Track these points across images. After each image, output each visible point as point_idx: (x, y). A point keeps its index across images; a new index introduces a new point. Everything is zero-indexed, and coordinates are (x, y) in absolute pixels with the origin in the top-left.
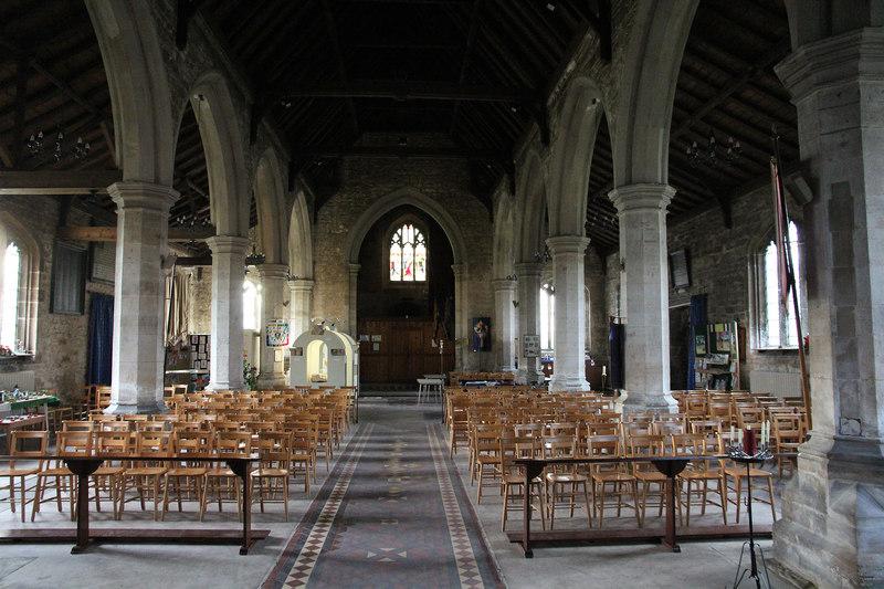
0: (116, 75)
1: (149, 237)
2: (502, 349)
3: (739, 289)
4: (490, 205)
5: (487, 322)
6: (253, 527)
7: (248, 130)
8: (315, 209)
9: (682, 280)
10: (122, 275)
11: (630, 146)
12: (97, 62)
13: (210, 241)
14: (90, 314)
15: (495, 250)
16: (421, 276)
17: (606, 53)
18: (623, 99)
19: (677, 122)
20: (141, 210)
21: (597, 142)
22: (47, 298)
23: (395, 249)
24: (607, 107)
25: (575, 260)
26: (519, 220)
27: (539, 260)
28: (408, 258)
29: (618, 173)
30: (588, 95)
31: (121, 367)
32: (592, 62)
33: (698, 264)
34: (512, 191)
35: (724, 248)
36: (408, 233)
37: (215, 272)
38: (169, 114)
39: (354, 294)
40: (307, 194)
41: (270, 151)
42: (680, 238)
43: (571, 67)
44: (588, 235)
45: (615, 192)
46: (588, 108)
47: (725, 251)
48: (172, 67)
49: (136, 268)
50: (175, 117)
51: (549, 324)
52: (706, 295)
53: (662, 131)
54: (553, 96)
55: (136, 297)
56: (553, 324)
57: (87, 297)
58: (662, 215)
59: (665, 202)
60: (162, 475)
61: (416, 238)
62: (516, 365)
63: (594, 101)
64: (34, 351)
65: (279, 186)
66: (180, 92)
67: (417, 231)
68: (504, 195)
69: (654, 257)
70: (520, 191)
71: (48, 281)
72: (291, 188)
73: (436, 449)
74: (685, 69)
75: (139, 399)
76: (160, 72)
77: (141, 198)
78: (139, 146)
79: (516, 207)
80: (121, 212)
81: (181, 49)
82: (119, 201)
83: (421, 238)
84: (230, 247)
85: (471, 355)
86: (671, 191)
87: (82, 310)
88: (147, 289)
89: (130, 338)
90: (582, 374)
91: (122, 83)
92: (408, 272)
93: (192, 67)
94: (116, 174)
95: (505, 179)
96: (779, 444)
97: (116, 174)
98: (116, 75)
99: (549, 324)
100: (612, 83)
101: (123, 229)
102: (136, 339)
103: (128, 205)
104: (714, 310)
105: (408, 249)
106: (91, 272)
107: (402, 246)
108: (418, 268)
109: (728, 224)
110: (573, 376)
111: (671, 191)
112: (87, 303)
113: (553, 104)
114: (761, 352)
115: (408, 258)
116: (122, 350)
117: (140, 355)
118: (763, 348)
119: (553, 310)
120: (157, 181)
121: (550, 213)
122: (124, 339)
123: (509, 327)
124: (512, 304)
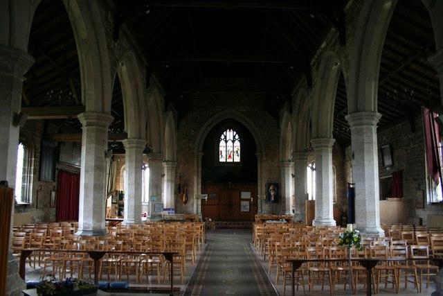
0: (84, 57)
1: (98, 142)
2: (285, 202)
3: (420, 168)
4: (278, 118)
5: (278, 187)
6: (174, 286)
7: (145, 81)
8: (179, 120)
9: (388, 162)
10: (85, 163)
11: (356, 95)
12: (73, 46)
13: (124, 141)
14: (58, 181)
15: (281, 144)
16: (237, 159)
17: (343, 40)
18: (353, 66)
19: (382, 75)
20: (95, 127)
21: (338, 90)
22: (38, 173)
23: (222, 143)
24: (344, 70)
25: (327, 152)
26: (295, 128)
27: (306, 151)
28: (230, 148)
29: (350, 107)
30: (331, 63)
31: (84, 210)
32: (335, 44)
33: (397, 153)
34: (291, 112)
35: (412, 145)
36: (230, 134)
37: (127, 159)
38: (109, 74)
39: (200, 170)
40: (174, 114)
41: (156, 90)
42: (387, 138)
43: (323, 45)
44: (334, 138)
45: (349, 116)
46: (333, 68)
47: (412, 146)
48: (111, 50)
49: (92, 157)
50: (112, 78)
51: (312, 187)
52: (402, 171)
53: (374, 83)
54: (313, 60)
55: (92, 174)
56: (316, 184)
57: (57, 172)
58: (374, 129)
59: (375, 122)
60: (140, 263)
61: (234, 137)
62: (293, 211)
63: (336, 64)
64: (31, 202)
65: (160, 110)
66: (114, 65)
67: (235, 133)
68: (286, 113)
69: (371, 152)
70: (295, 111)
71: (38, 164)
72: (166, 110)
73: (250, 256)
74: (385, 46)
75: (93, 228)
76: (105, 54)
77: (95, 121)
78: (93, 96)
79: (293, 121)
80: (84, 128)
81: (115, 42)
82: (83, 122)
83: (237, 137)
84: (135, 145)
85: (267, 205)
86: (379, 115)
87: (54, 179)
88: (98, 168)
89: (89, 195)
90: (331, 216)
91: (87, 63)
92: (230, 157)
93: (120, 50)
94: (82, 108)
95: (286, 103)
96: (434, 254)
97: (82, 108)
98: (84, 57)
99: (312, 187)
100: (346, 56)
101: (85, 137)
102: (92, 196)
103: (88, 124)
104: (406, 180)
105: (230, 143)
106: (58, 158)
107: (226, 142)
108: (235, 154)
109: (414, 131)
110: (327, 216)
111: (379, 115)
112: (56, 175)
113: (314, 65)
114: (433, 204)
115: (230, 148)
116: (85, 201)
117: (94, 204)
118: (434, 201)
119: (314, 179)
120: (103, 112)
121: (313, 125)
122: (86, 196)
123: (289, 189)
124: (291, 176)
